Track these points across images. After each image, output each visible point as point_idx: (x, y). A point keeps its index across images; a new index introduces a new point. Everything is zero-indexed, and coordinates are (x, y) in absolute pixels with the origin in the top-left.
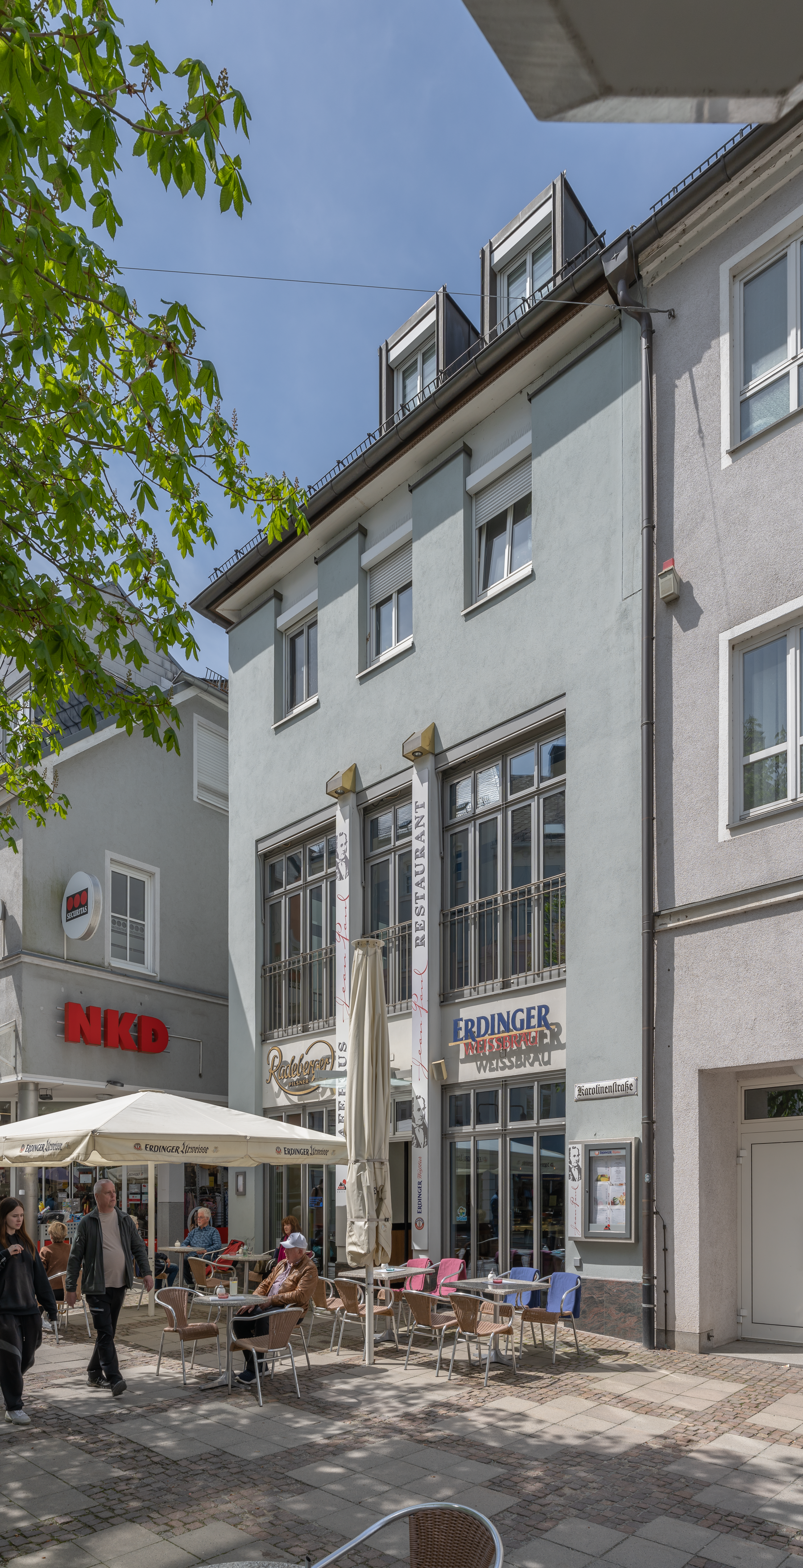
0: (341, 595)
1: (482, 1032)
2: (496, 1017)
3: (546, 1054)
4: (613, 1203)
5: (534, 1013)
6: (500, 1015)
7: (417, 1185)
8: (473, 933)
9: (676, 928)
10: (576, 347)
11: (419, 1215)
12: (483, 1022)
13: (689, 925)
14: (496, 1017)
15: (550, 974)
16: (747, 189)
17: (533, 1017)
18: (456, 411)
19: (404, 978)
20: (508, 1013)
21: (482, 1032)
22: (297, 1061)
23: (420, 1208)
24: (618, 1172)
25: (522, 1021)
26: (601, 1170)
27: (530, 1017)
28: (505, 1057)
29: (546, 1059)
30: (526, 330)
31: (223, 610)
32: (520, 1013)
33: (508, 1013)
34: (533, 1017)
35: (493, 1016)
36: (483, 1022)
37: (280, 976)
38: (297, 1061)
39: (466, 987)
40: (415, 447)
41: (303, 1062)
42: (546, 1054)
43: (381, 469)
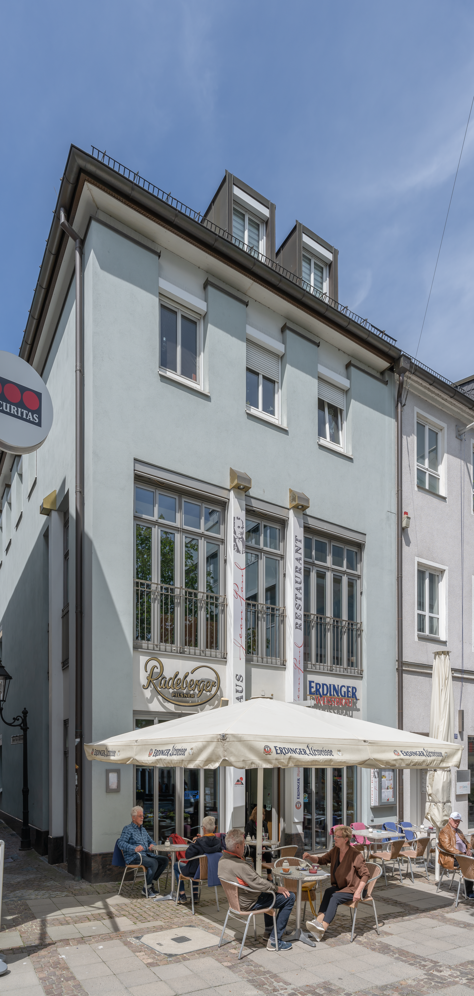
0: (232, 335)
1: (325, 693)
2: (332, 686)
3: (351, 712)
4: (388, 789)
5: (350, 689)
6: (334, 686)
7: (297, 781)
8: (345, 637)
9: (407, 670)
10: (373, 369)
11: (298, 800)
12: (325, 687)
13: (422, 673)
14: (332, 686)
15: (353, 671)
16: (436, 397)
17: (313, 687)
18: (152, 220)
19: (212, 633)
20: (338, 686)
21: (325, 693)
22: (181, 676)
23: (298, 795)
24: (389, 774)
25: (345, 692)
26: (383, 773)
27: (348, 691)
28: (331, 709)
29: (351, 715)
30: (305, 300)
31: (89, 189)
32: (343, 688)
33: (338, 686)
34: (313, 687)
35: (330, 685)
36: (325, 687)
37: (149, 594)
38: (181, 676)
39: (309, 662)
40: (299, 310)
41: (188, 679)
42: (351, 712)
43: (280, 294)
